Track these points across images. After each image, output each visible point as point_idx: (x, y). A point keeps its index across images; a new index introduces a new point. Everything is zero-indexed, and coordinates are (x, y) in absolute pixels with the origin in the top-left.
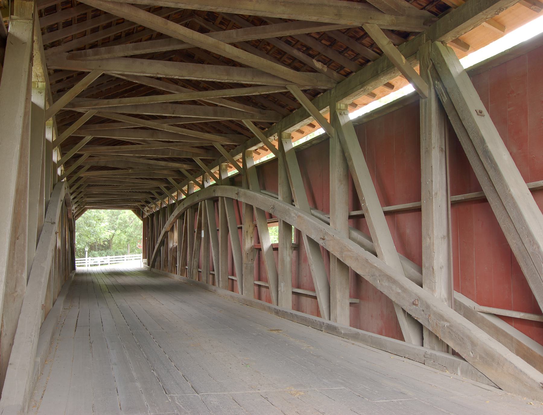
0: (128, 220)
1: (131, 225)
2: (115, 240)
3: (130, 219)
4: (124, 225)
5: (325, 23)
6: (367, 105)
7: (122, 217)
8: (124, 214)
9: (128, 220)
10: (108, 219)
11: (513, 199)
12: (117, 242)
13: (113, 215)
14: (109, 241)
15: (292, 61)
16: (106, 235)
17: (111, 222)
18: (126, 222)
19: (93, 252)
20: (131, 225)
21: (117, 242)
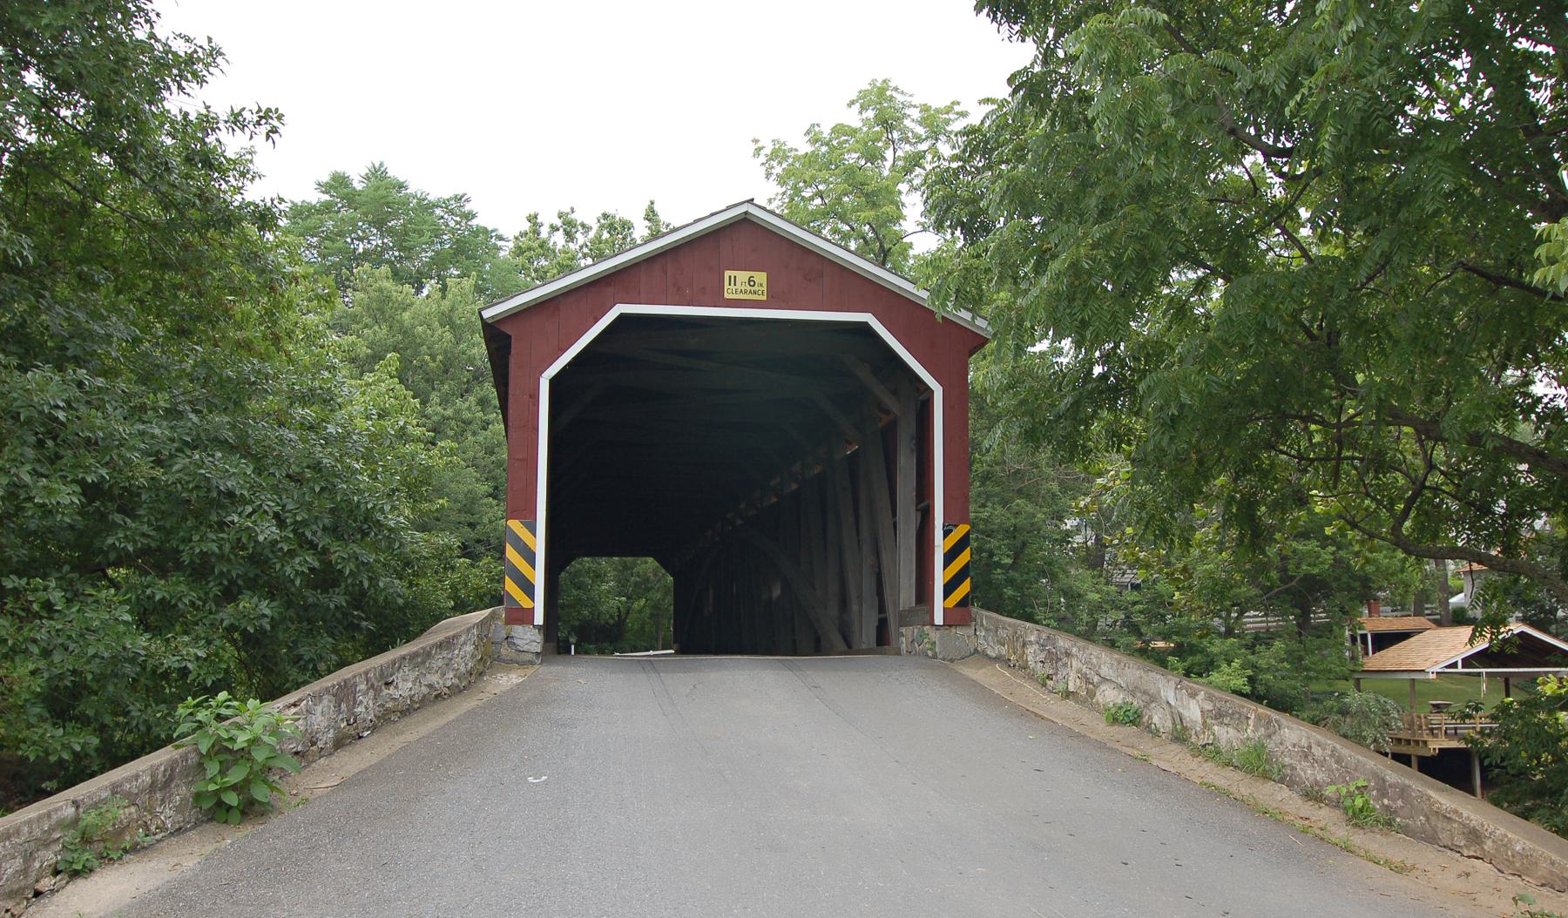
0: (652, 578)
1: (658, 585)
2: (633, 625)
3: (655, 575)
4: (643, 587)
5: (507, 365)
6: (986, 97)
7: (641, 571)
8: (643, 566)
9: (652, 578)
10: (615, 576)
11: (1156, 660)
12: (636, 627)
13: (625, 567)
14: (621, 622)
15: (1427, 484)
16: (614, 603)
17: (622, 582)
18: (648, 580)
19: (586, 646)
20: (658, 585)
21: (636, 627)
